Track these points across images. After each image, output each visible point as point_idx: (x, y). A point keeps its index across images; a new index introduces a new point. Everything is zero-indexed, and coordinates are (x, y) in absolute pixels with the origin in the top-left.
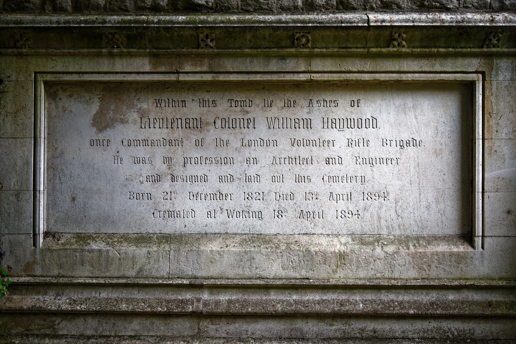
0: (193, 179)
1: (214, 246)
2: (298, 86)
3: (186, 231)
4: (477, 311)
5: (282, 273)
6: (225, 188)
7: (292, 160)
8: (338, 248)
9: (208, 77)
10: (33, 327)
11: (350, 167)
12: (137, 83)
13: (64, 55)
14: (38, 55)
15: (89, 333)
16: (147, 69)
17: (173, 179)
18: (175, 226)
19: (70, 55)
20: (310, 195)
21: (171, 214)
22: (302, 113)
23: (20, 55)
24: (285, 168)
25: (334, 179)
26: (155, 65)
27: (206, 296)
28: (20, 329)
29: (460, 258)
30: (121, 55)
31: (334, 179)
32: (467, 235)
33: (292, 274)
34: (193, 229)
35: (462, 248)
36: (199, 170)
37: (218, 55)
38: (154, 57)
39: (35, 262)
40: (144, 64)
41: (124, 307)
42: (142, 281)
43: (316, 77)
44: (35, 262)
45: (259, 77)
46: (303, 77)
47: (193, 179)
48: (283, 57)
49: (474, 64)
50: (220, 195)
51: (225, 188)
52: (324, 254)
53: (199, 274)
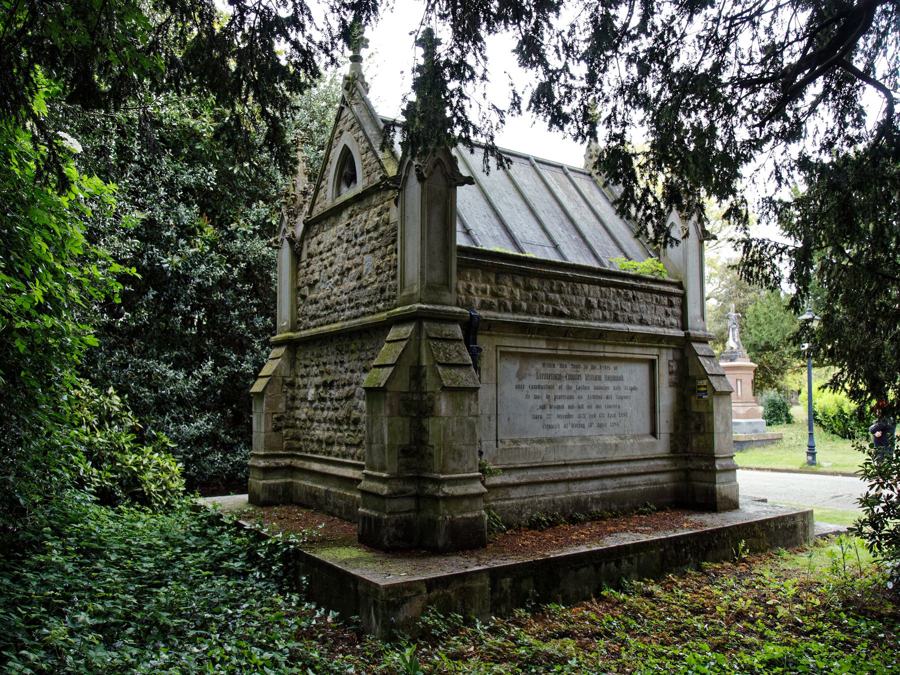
0: (559, 407)
1: (570, 443)
2: (597, 359)
3: (556, 436)
4: (662, 469)
5: (597, 456)
6: (571, 412)
7: (595, 397)
8: (614, 442)
9: (568, 353)
10: (500, 494)
11: (614, 401)
12: (536, 353)
13: (509, 337)
14: (498, 336)
15: (524, 495)
16: (545, 346)
17: (551, 407)
18: (551, 433)
19: (513, 337)
20: (602, 415)
21: (550, 427)
22: (597, 372)
23: (490, 335)
24: (592, 401)
25: (609, 407)
26: (548, 345)
27: (570, 470)
28: (494, 497)
29: (653, 444)
30: (535, 339)
31: (609, 407)
32: (654, 433)
33: (600, 456)
34: (559, 435)
35: (653, 440)
36: (559, 402)
37: (572, 341)
38: (548, 340)
39: (498, 457)
40: (543, 344)
41: (541, 479)
42: (546, 464)
43: (607, 355)
44: (498, 457)
45: (587, 354)
46: (602, 354)
47: (559, 407)
48: (595, 344)
49: (655, 351)
50: (569, 416)
51: (571, 412)
52: (610, 445)
53: (567, 458)
